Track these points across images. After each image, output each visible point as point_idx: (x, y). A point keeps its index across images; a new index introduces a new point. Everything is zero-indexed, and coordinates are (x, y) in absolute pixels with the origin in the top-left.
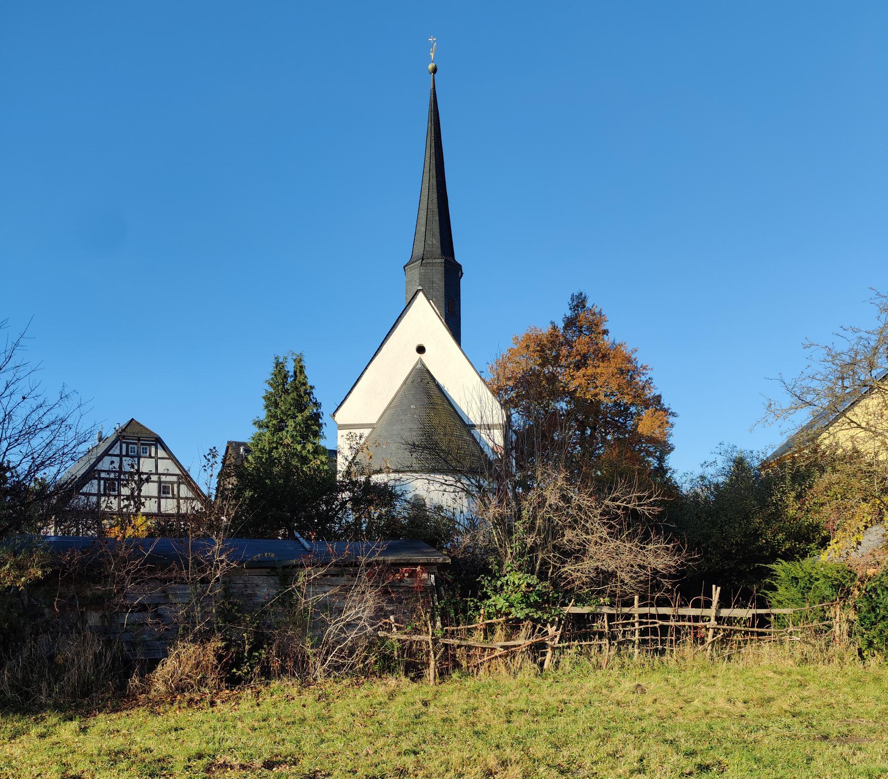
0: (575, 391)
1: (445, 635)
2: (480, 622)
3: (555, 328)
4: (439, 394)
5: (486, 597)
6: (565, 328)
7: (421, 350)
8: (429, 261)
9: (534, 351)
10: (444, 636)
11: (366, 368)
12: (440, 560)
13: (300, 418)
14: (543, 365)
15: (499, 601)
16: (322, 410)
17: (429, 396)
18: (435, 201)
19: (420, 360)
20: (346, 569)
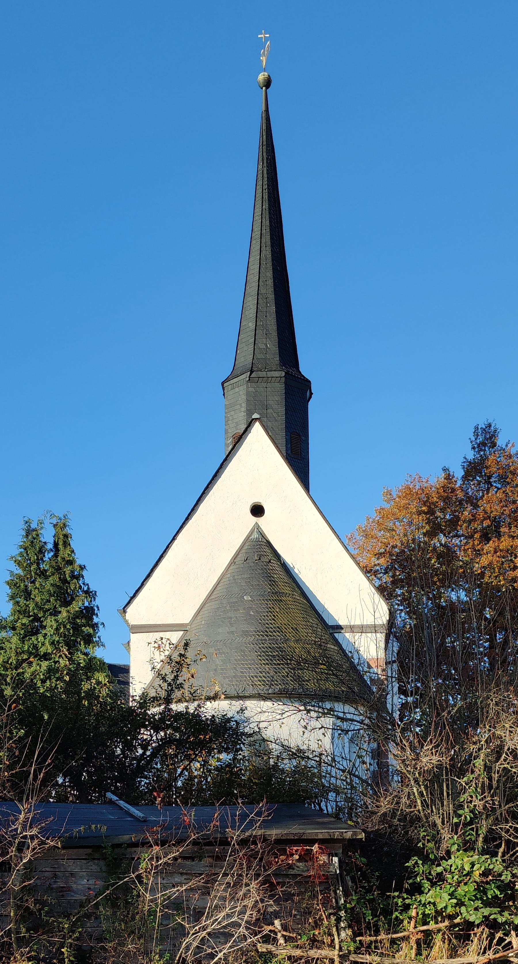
0: (482, 575)
1: (358, 948)
2: (410, 928)
3: (449, 477)
4: (286, 579)
5: (417, 889)
6: (465, 478)
7: (257, 510)
8: (261, 374)
9: (419, 513)
10: (357, 951)
11: (174, 539)
12: (349, 835)
13: (64, 614)
14: (432, 534)
15: (439, 897)
16: (98, 602)
17: (272, 582)
18: (270, 282)
19: (257, 527)
20: (210, 849)
